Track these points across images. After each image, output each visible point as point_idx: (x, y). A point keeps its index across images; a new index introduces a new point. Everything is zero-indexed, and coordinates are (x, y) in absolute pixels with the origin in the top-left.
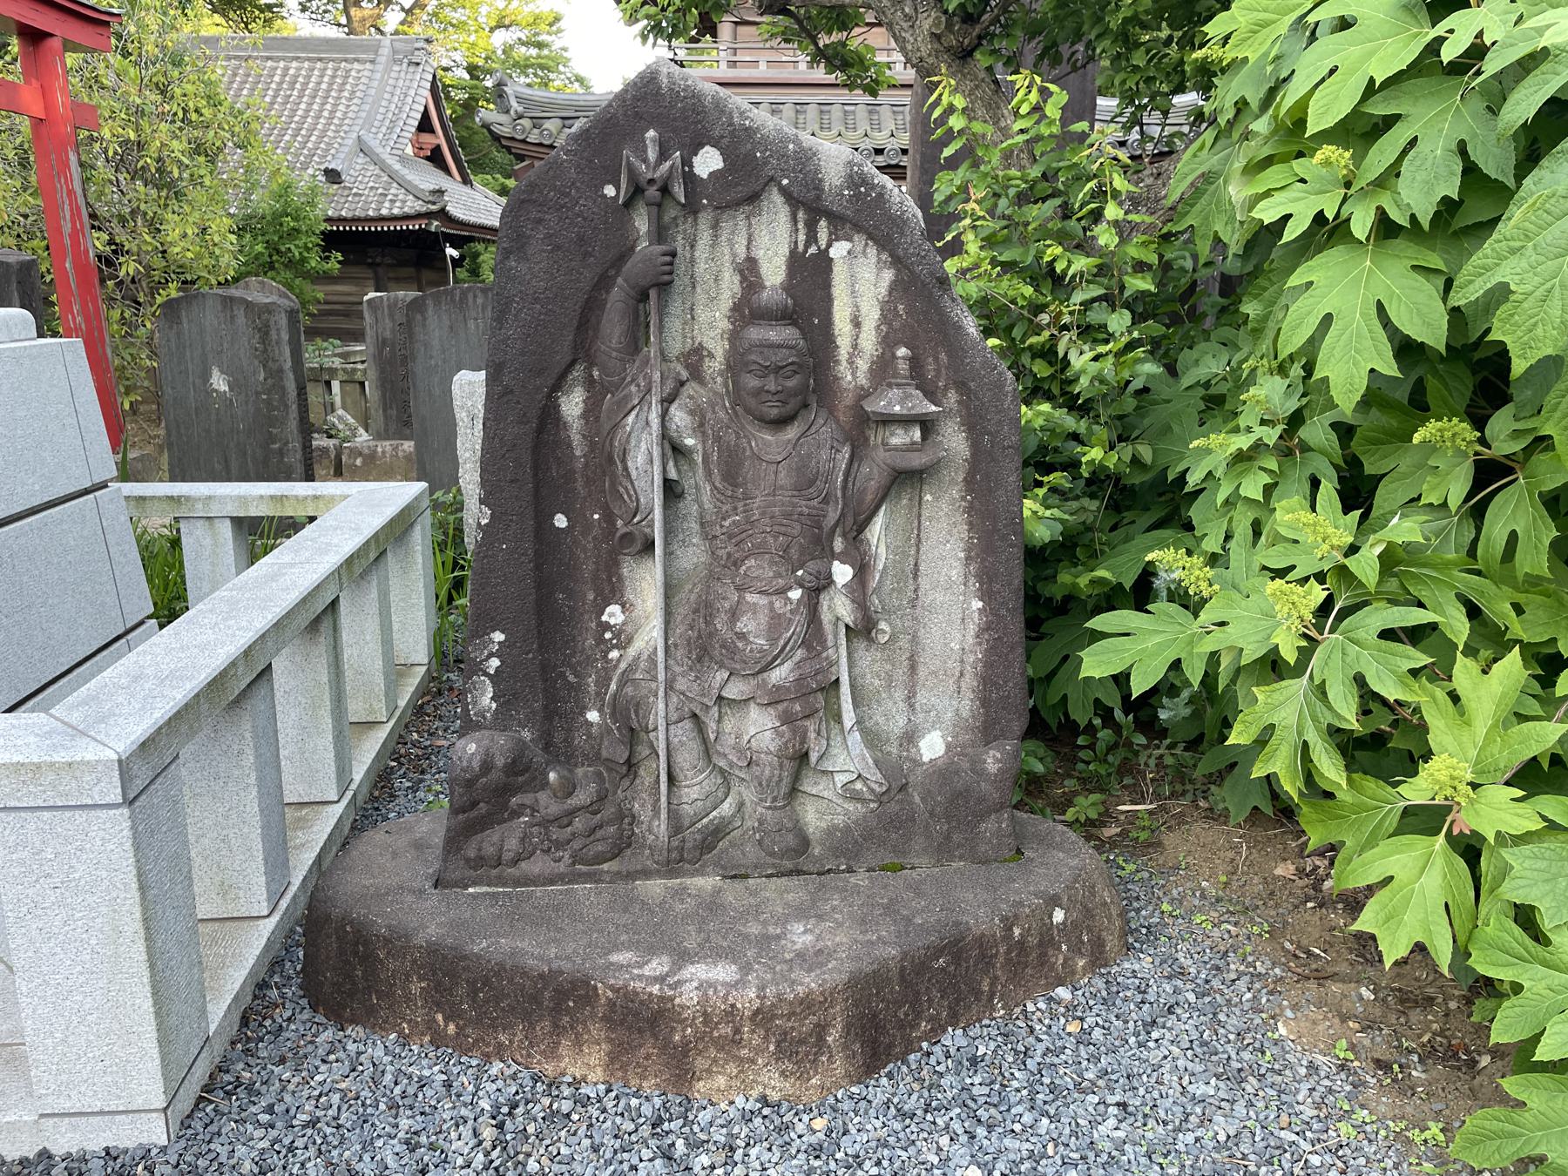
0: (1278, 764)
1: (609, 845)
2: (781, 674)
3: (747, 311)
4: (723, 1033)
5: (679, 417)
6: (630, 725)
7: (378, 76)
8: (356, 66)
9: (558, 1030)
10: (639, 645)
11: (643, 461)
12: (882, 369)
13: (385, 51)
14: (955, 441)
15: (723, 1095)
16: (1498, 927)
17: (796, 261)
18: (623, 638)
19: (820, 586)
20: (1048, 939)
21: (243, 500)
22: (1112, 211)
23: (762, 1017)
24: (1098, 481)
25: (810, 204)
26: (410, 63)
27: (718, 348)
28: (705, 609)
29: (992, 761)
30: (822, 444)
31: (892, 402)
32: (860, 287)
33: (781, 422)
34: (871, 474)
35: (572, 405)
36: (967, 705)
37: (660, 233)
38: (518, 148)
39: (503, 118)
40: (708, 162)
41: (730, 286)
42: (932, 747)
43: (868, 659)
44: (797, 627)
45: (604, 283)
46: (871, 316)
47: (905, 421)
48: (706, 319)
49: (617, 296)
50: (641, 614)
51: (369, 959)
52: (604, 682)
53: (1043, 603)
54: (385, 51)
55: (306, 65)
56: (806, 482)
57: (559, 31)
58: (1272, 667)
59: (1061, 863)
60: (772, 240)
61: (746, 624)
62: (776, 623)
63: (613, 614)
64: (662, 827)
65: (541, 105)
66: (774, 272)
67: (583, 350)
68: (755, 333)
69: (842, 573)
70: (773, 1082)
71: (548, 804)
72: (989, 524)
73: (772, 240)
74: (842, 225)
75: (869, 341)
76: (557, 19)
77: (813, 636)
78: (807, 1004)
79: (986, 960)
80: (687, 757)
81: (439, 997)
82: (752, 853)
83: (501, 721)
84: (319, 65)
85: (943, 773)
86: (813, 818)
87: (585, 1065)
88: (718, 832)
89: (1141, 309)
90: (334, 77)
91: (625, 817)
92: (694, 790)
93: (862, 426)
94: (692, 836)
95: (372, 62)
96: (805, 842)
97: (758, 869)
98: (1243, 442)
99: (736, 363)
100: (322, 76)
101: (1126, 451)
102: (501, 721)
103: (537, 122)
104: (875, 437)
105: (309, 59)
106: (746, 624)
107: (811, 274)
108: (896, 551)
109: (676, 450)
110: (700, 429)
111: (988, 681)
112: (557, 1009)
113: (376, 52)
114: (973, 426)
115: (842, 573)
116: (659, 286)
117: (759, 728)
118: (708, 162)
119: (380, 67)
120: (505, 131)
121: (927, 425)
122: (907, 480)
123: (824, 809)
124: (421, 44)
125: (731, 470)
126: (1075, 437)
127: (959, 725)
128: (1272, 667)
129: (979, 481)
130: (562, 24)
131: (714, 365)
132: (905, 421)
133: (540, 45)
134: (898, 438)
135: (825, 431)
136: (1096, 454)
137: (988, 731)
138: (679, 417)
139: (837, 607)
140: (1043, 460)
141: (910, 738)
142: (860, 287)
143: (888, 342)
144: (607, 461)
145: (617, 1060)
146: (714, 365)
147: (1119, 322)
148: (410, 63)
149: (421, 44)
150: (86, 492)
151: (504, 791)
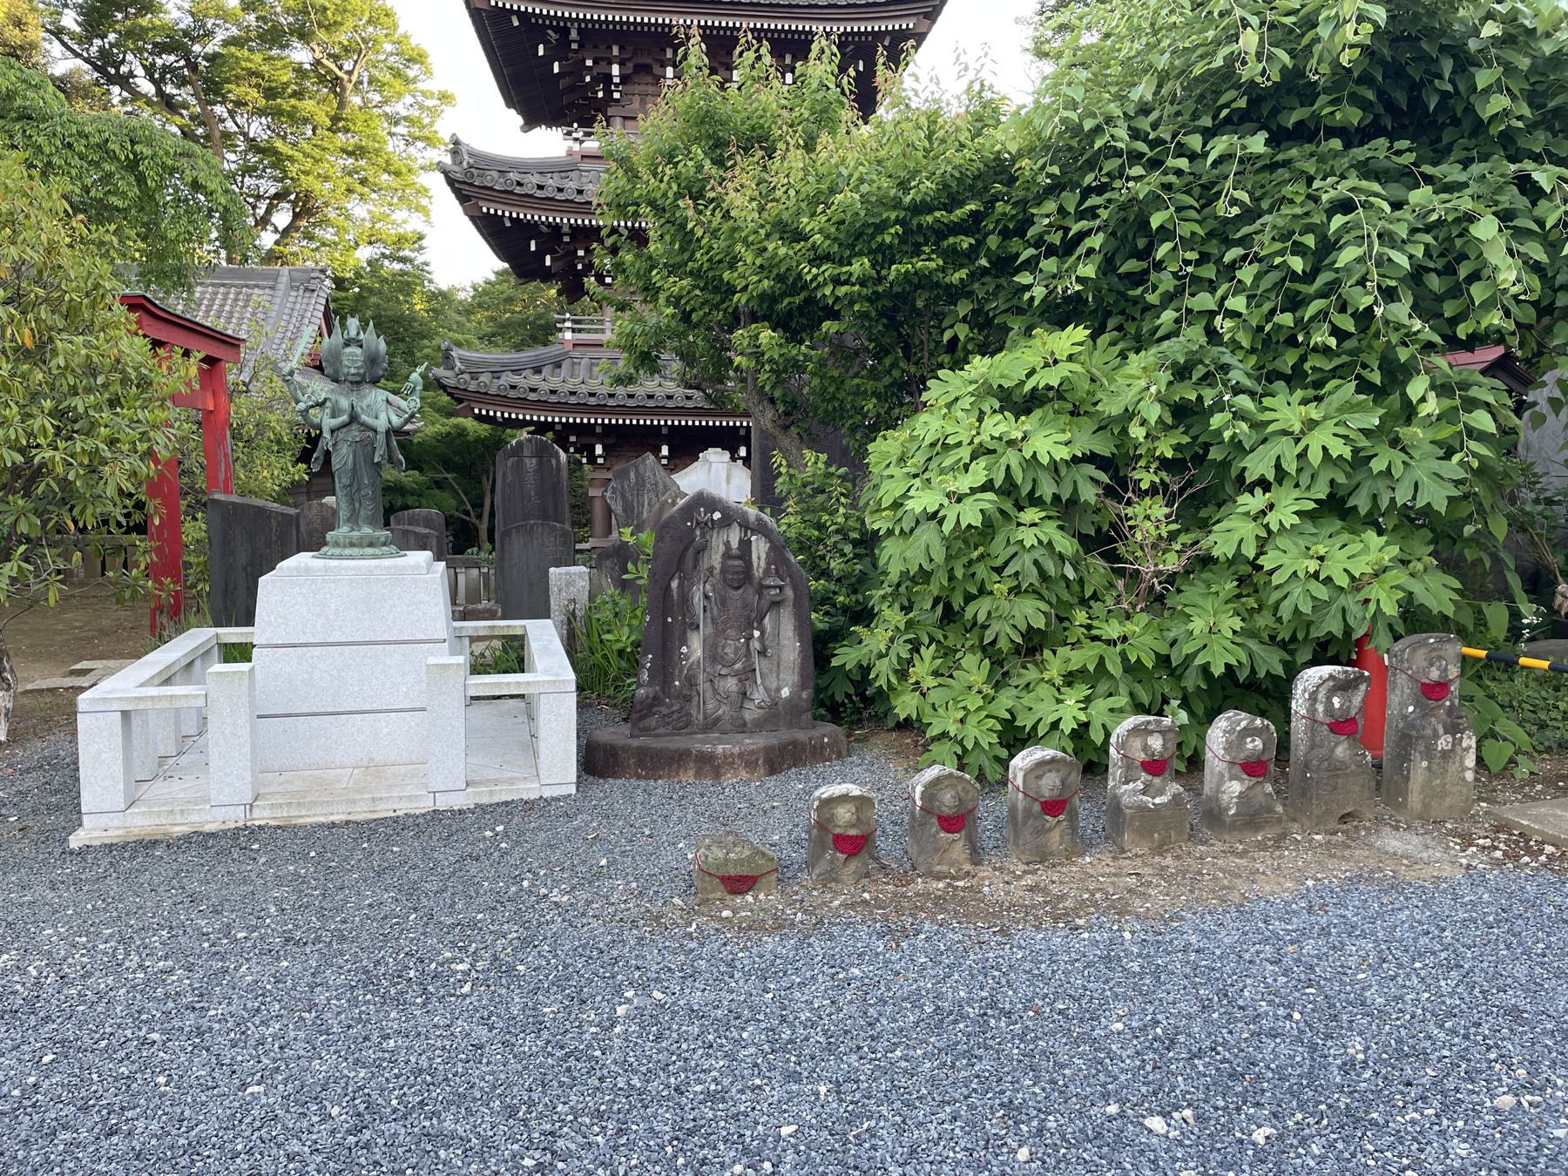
0: (882, 682)
1: (683, 724)
2: (737, 666)
3: (727, 555)
4: (729, 761)
5: (708, 587)
6: (691, 682)
7: (278, 300)
8: (256, 291)
9: (679, 767)
10: (693, 658)
11: (698, 599)
12: (767, 572)
13: (284, 279)
14: (789, 593)
15: (729, 779)
16: (928, 710)
17: (741, 541)
18: (687, 657)
19: (750, 638)
20: (823, 746)
21: (476, 628)
22: (842, 510)
23: (741, 755)
24: (845, 609)
25: (745, 526)
26: (306, 289)
27: (718, 566)
28: (715, 646)
29: (804, 695)
30: (750, 594)
31: (770, 582)
32: (760, 548)
33: (737, 588)
34: (765, 603)
35: (675, 584)
36: (796, 678)
37: (703, 535)
38: (458, 394)
39: (449, 373)
40: (717, 516)
41: (722, 548)
42: (785, 692)
43: (765, 662)
44: (743, 651)
45: (686, 549)
46: (763, 556)
47: (774, 587)
48: (715, 558)
49: (690, 552)
50: (695, 648)
51: (615, 756)
52: (681, 671)
53: (820, 648)
54: (284, 279)
55: (210, 289)
56: (745, 606)
57: (421, 248)
58: (881, 656)
59: (828, 732)
60: (734, 536)
61: (727, 650)
62: (737, 649)
63: (684, 649)
64: (701, 717)
65: (477, 364)
66: (735, 544)
67: (679, 568)
68: (731, 562)
69: (757, 634)
70: (744, 774)
71: (664, 710)
72: (802, 623)
73: (734, 536)
74: (754, 532)
75: (763, 564)
76: (421, 238)
77: (748, 655)
78: (753, 752)
79: (804, 750)
80: (709, 694)
81: (640, 763)
82: (729, 727)
83: (650, 684)
84: (222, 290)
85: (788, 700)
86: (748, 716)
87: (688, 777)
88: (718, 719)
89: (855, 543)
90: (236, 300)
91: (689, 714)
92: (710, 706)
93: (762, 588)
94: (710, 720)
95: (272, 288)
96: (745, 724)
97: (731, 731)
98: (882, 592)
99: (724, 571)
100: (225, 299)
101: (854, 598)
102: (650, 684)
103: (474, 376)
104: (765, 592)
105: (213, 285)
106: (727, 650)
107: (745, 545)
108: (773, 628)
109: (706, 597)
110: (714, 590)
111: (802, 668)
112: (680, 760)
113: (276, 280)
114: (795, 588)
115: (757, 634)
116: (703, 548)
117: (731, 684)
118: (717, 516)
119: (280, 293)
120: (452, 382)
121: (781, 588)
122: (776, 604)
123: (751, 713)
124: (317, 274)
125: (723, 602)
126: (835, 593)
127: (793, 685)
128: (881, 656)
129: (797, 605)
130: (424, 243)
131: (717, 572)
132: (774, 587)
133: (403, 260)
134: (773, 592)
135: (751, 591)
136: (841, 599)
137: (803, 687)
138: (708, 587)
139: (756, 645)
140: (826, 599)
141: (778, 690)
142: (760, 548)
143: (768, 564)
144: (685, 599)
145: (698, 775)
146: (717, 572)
147: (848, 549)
148: (306, 289)
149: (317, 274)
150: (294, 646)
151: (652, 706)
